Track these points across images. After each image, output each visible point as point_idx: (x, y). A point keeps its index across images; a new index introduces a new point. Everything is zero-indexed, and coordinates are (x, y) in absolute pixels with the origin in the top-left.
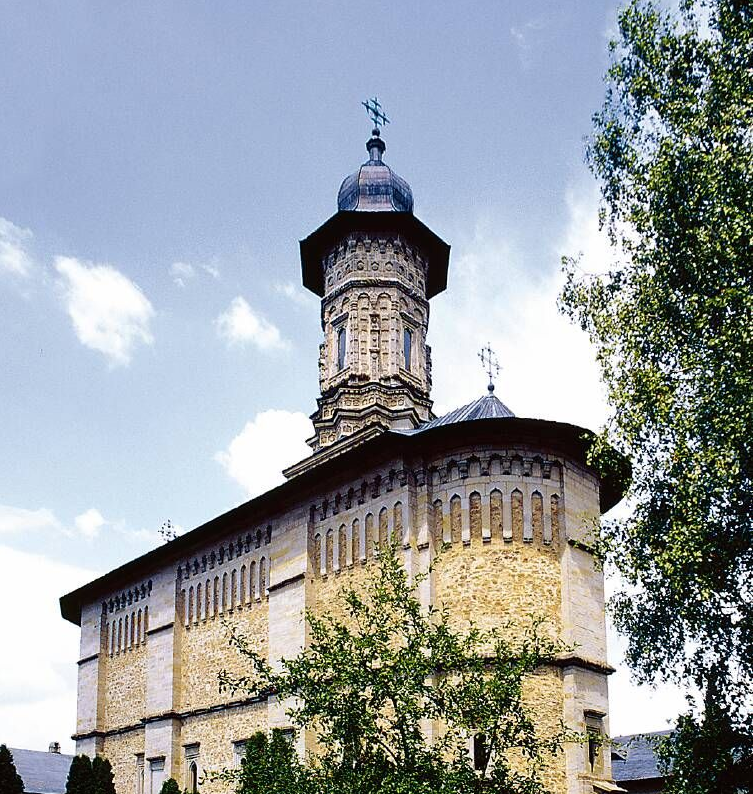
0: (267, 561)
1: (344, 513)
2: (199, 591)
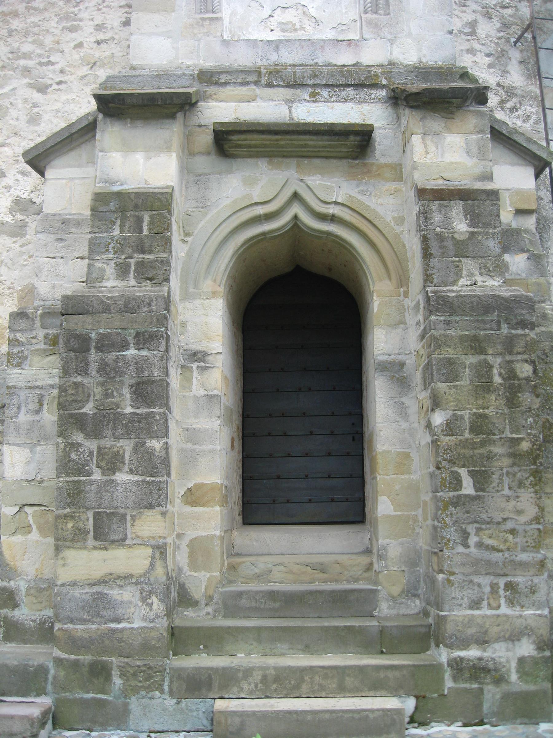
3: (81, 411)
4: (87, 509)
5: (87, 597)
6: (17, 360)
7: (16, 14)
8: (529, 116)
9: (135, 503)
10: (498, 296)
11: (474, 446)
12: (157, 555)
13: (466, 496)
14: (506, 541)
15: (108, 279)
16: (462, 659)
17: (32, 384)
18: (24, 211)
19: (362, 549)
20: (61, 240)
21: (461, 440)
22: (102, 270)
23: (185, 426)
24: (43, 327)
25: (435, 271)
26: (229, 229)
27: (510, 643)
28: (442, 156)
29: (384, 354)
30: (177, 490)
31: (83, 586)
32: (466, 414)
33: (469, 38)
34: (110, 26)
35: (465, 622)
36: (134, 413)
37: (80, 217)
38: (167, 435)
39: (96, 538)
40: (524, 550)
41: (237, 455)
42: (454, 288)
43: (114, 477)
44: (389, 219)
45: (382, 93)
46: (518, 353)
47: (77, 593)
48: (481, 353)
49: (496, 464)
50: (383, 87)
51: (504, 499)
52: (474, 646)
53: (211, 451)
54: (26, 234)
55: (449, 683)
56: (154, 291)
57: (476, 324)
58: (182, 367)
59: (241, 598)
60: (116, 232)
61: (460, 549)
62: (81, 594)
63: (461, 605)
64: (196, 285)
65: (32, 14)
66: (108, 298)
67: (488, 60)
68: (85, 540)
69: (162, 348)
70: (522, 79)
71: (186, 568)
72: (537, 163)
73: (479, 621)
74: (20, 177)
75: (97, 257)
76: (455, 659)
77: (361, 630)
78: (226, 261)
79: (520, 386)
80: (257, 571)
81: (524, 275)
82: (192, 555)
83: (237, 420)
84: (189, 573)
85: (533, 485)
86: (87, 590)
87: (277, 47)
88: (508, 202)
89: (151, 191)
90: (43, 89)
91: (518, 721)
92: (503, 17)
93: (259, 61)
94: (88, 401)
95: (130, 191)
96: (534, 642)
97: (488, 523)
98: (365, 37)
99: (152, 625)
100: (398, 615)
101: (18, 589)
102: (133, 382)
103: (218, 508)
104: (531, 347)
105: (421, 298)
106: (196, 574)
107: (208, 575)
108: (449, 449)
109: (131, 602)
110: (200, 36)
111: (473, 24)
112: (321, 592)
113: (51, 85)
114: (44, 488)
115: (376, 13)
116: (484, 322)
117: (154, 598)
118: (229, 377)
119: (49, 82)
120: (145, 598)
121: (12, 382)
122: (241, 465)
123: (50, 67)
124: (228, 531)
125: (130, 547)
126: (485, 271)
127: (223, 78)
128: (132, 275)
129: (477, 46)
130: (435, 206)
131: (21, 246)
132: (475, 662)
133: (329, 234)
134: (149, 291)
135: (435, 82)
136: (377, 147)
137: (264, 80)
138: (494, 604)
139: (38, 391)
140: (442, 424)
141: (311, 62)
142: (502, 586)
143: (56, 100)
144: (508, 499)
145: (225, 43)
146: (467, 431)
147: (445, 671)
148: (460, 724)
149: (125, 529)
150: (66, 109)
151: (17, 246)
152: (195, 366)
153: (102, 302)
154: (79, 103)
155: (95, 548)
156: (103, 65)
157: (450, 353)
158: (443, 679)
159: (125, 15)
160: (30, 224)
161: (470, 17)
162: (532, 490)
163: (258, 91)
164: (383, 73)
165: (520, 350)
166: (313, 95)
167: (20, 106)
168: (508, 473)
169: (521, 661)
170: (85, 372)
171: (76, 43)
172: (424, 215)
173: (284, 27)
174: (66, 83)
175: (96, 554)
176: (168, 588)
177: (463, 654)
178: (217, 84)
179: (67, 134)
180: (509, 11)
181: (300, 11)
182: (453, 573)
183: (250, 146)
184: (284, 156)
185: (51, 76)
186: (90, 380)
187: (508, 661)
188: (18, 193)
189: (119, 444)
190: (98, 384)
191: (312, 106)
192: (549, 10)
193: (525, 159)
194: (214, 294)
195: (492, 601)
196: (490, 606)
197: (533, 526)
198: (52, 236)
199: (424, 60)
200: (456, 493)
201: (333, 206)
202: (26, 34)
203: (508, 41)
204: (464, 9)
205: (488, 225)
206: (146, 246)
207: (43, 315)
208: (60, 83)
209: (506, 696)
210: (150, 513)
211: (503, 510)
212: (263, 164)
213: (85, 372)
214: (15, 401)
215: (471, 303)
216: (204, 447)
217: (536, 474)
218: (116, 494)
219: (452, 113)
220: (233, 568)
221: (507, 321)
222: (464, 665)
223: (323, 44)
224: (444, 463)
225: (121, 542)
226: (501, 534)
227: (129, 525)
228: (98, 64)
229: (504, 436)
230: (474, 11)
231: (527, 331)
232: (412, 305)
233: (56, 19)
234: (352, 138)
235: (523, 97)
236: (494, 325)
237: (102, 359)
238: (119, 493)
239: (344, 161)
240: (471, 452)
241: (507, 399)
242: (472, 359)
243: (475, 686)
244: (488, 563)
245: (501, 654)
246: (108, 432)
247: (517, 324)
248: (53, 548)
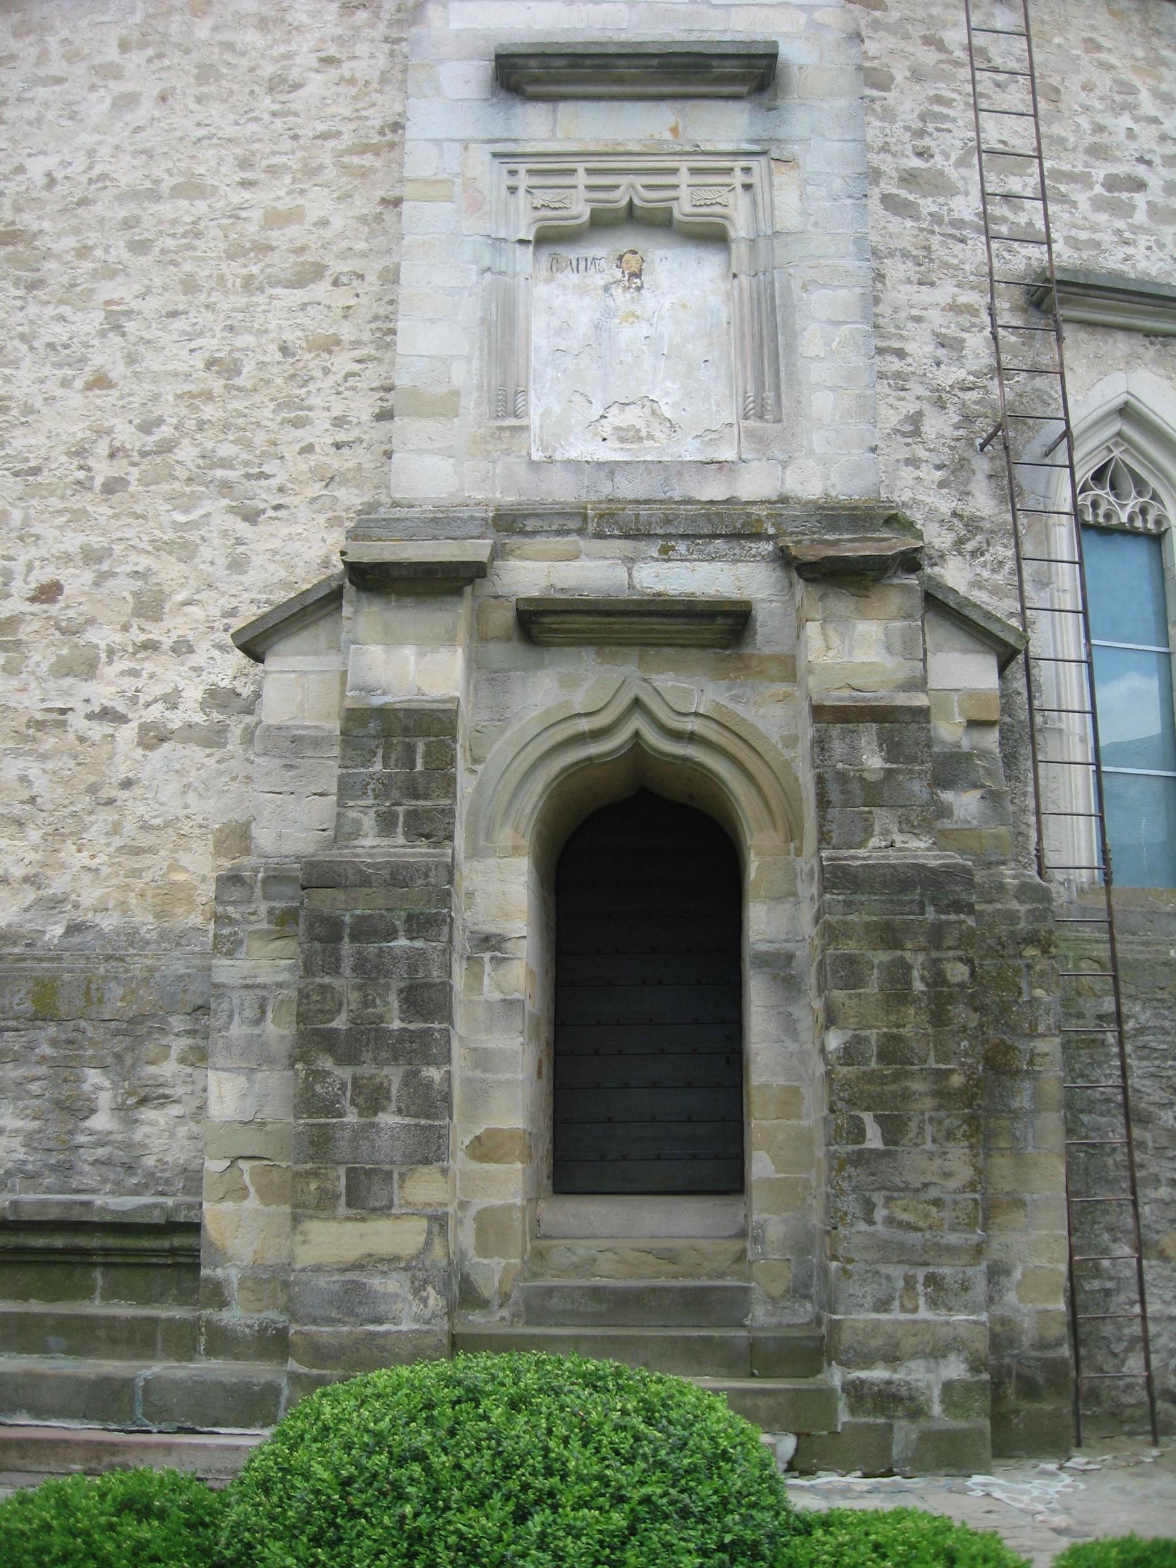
3: (331, 1025)
4: (338, 1163)
5: (336, 1287)
6: (229, 946)
7: (208, 396)
8: (1001, 563)
9: (405, 1156)
10: (923, 866)
11: (882, 1080)
12: (436, 1230)
13: (871, 1151)
14: (927, 1216)
15: (366, 836)
16: (862, 1382)
17: (249, 982)
18: (223, 707)
19: (733, 1231)
20: (290, 767)
21: (864, 1073)
22: (358, 822)
23: (472, 1045)
24: (267, 897)
25: (834, 826)
26: (537, 754)
27: (932, 1360)
28: (850, 653)
29: (763, 941)
30: (459, 1139)
31: (330, 1272)
32: (873, 1034)
33: (909, 440)
34: (355, 421)
35: (868, 1330)
36: (405, 1030)
37: (320, 734)
38: (449, 1061)
39: (349, 1205)
40: (953, 1229)
41: (546, 1085)
42: (861, 852)
43: (376, 1120)
44: (775, 739)
45: (768, 547)
46: (949, 948)
47: (322, 1281)
48: (895, 948)
49: (915, 1106)
50: (770, 538)
51: (925, 1156)
52: (880, 1364)
53: (509, 1082)
54: (226, 743)
55: (844, 1416)
56: (433, 855)
57: (889, 906)
58: (469, 958)
59: (551, 1297)
60: (378, 767)
61: (862, 1226)
62: (328, 1283)
63: (862, 1306)
64: (489, 836)
65: (234, 397)
66: (368, 865)
67: (938, 475)
68: (334, 1207)
69: (444, 938)
70: (993, 503)
71: (472, 1252)
72: (1002, 650)
73: (888, 1328)
74: (216, 653)
75: (351, 803)
76: (853, 1382)
77: (724, 1343)
78: (534, 799)
79: (950, 995)
80: (575, 1259)
81: (975, 823)
82: (480, 1233)
83: (546, 1032)
84: (476, 1259)
85: (967, 1137)
86: (336, 1277)
87: (612, 473)
88: (956, 709)
89: (428, 706)
90: (251, 517)
91: (942, 1472)
92: (964, 405)
93: (584, 494)
94: (339, 1011)
95: (397, 706)
96: (966, 1360)
97: (902, 1190)
98: (744, 457)
99: (427, 1327)
100: (780, 1325)
101: (227, 1280)
102: (402, 985)
103: (519, 1165)
104: (967, 939)
105: (814, 862)
106: (486, 1261)
107: (503, 1262)
108: (847, 1084)
109: (397, 1295)
110: (495, 455)
111: (916, 419)
112: (668, 1290)
113: (264, 511)
114: (267, 1133)
115: (761, 417)
116: (901, 903)
117: (430, 1289)
118: (536, 969)
119: (262, 506)
120: (417, 1290)
121: (219, 977)
122: (551, 1101)
123: (263, 483)
124: (533, 1200)
125: (397, 1217)
126: (908, 826)
127: (530, 525)
128: (400, 830)
129: (922, 453)
130: (836, 730)
131: (218, 762)
132: (882, 1386)
133: (685, 759)
134: (422, 855)
135: (848, 531)
136: (759, 630)
137: (591, 527)
138: (909, 1305)
139: (260, 992)
140: (837, 1049)
141: (662, 496)
142: (921, 1279)
143: (272, 535)
144: (931, 1156)
145: (534, 465)
146: (874, 1059)
147: (838, 1399)
148: (859, 1473)
149: (391, 1193)
150: (288, 550)
151: (211, 762)
152: (487, 956)
153: (360, 871)
154: (307, 540)
155: (348, 1219)
156: (345, 482)
157: (851, 947)
158: (836, 1409)
159: (380, 403)
160: (232, 728)
161: (911, 407)
162: (966, 1144)
163: (583, 544)
164: (769, 516)
165: (951, 943)
166: (665, 550)
167: (216, 542)
168: (931, 1119)
169: (948, 1386)
170: (336, 971)
171: (303, 445)
172: (821, 744)
173: (627, 436)
174: (287, 507)
175: (349, 1226)
176: (449, 1276)
177: (863, 1374)
178: (522, 533)
179: (298, 607)
180: (974, 395)
181: (647, 410)
182: (850, 1261)
183: (570, 631)
184: (620, 644)
185: (264, 496)
186: (342, 981)
187: (928, 1386)
188: (213, 678)
189: (384, 1073)
190: (353, 988)
191: (662, 568)
192: (1039, 390)
193: (984, 644)
194: (516, 850)
195: (906, 1302)
196: (903, 1308)
197: (968, 1195)
198: (278, 761)
199: (833, 493)
200: (857, 1147)
201: (692, 718)
202: (226, 428)
203: (970, 443)
204: (902, 394)
205: (912, 759)
206: (421, 788)
207: (267, 880)
208: (277, 507)
209: (925, 1437)
210: (425, 1169)
211: (923, 1172)
212: (589, 656)
213: (336, 971)
214: (225, 1006)
215: (884, 875)
216: (500, 1076)
217: (971, 1120)
218: (378, 1143)
219: (866, 588)
220: (539, 1254)
221: (934, 901)
222: (866, 1390)
223: (681, 468)
224: (840, 1105)
225: (384, 1210)
226: (921, 1206)
227: (396, 1186)
228: (337, 479)
229: (926, 1066)
230: (918, 398)
231: (962, 916)
232: (806, 868)
233: (272, 406)
234: (720, 620)
235: (992, 532)
236: (916, 909)
237: (359, 952)
238: (383, 1141)
239: (710, 651)
240: (878, 1089)
241: (932, 1013)
242: (882, 957)
243: (881, 1420)
244: (902, 1246)
245: (918, 1376)
246: (367, 1056)
247: (948, 906)
248: (289, 1218)
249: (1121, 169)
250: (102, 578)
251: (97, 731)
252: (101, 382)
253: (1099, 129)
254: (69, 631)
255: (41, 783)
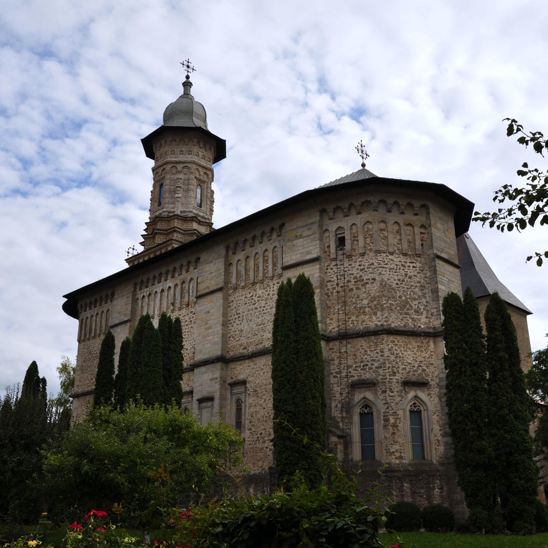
0: (279, 250)
1: (248, 249)
2: (102, 315)
111: (337, 405)
161: (336, 404)
249: (365, 364)
250: (266, 432)
251: (266, 449)
252: (264, 408)
253: (362, 358)
254: (263, 438)
255: (262, 456)
